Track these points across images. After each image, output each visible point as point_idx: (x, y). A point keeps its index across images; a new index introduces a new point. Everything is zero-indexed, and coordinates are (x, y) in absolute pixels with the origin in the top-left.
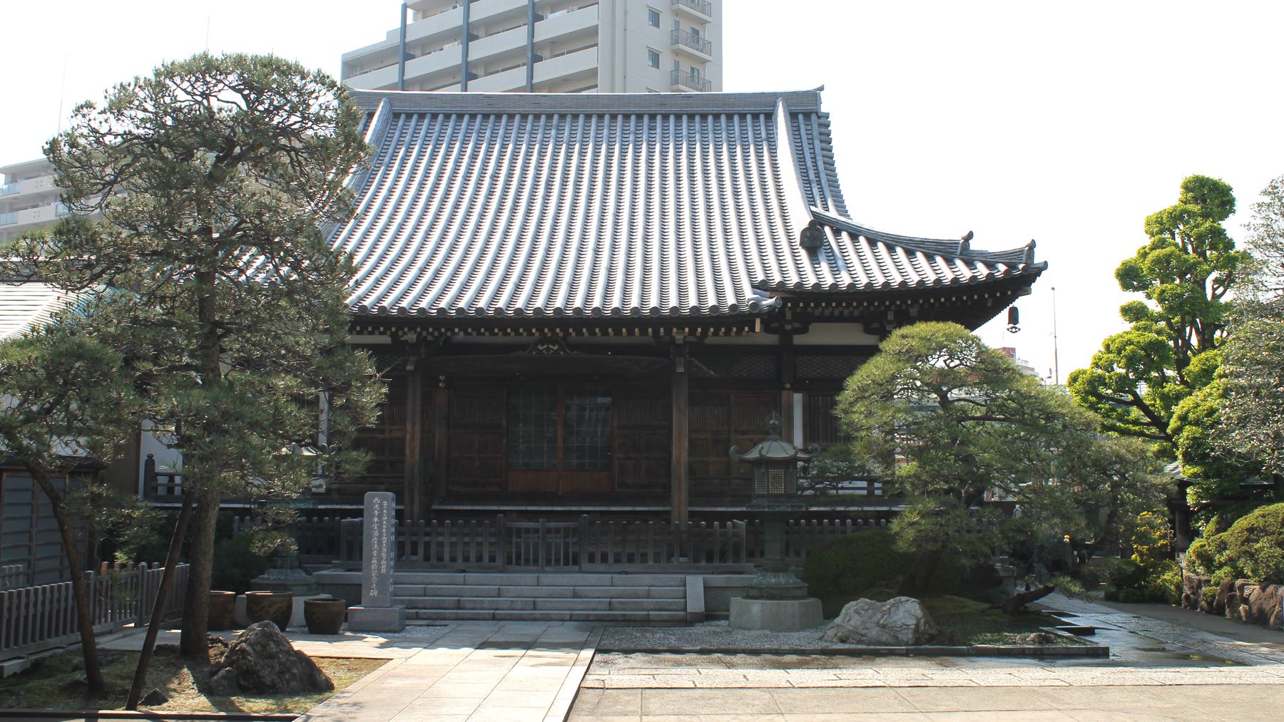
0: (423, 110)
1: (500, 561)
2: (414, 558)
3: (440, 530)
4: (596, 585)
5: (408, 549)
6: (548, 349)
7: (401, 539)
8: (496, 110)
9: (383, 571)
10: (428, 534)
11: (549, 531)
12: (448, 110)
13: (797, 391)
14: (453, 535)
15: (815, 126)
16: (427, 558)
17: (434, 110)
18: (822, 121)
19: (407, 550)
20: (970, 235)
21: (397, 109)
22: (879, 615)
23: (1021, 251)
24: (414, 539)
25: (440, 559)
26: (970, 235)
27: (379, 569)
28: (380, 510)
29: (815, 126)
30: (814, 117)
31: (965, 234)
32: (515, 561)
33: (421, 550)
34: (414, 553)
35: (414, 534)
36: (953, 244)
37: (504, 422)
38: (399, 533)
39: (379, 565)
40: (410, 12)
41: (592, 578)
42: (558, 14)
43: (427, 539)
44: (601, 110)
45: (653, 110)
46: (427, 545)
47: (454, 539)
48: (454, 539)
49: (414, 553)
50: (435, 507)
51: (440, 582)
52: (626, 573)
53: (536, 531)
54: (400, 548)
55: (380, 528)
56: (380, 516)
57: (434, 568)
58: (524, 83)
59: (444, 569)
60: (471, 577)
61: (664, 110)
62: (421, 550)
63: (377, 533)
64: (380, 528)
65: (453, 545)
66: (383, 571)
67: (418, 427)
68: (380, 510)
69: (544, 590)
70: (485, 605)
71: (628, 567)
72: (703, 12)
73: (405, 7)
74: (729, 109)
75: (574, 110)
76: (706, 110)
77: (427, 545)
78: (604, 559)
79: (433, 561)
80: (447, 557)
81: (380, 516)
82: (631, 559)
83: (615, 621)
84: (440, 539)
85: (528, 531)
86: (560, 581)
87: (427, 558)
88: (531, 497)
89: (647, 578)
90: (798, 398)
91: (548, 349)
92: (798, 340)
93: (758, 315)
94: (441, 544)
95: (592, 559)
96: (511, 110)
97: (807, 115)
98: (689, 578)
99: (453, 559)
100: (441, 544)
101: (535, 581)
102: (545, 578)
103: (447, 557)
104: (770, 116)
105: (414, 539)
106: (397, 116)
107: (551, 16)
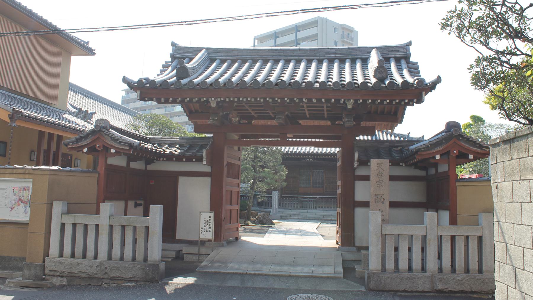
1: (299, 207)
4: (320, 212)
11: (310, 201)
16: (283, 206)
19: (281, 205)
20: (409, 133)
26: (409, 133)
28: (276, 195)
32: (302, 207)
36: (405, 135)
38: (279, 201)
40: (256, 41)
41: (319, 211)
42: (304, 43)
51: (287, 212)
53: (307, 201)
54: (280, 204)
57: (284, 209)
58: (273, 45)
59: (287, 209)
60: (293, 210)
65: (288, 204)
68: (276, 195)
71: (327, 209)
72: (352, 41)
73: (255, 39)
78: (322, 207)
79: (285, 208)
82: (328, 207)
83: (325, 220)
85: (305, 201)
86: (314, 212)
88: (305, 194)
89: (332, 212)
94: (286, 204)
95: (319, 207)
102: (309, 211)
104: (365, 61)
107: (302, 43)
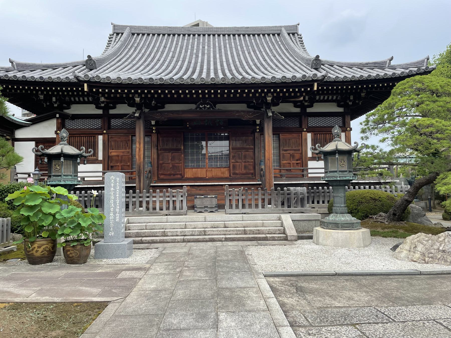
0: (144, 32)
2: (141, 209)
3: (154, 195)
5: (131, 206)
6: (205, 107)
7: (128, 200)
8: (173, 32)
9: (117, 220)
10: (148, 197)
12: (154, 32)
13: (308, 132)
14: (160, 197)
15: (297, 38)
17: (148, 32)
18: (299, 36)
20: (392, 59)
21: (133, 32)
22: (438, 244)
23: (423, 61)
24: (141, 199)
25: (154, 209)
26: (392, 59)
27: (115, 219)
29: (297, 38)
30: (296, 35)
31: (390, 57)
33: (144, 205)
34: (141, 206)
35: (140, 197)
37: (182, 148)
39: (115, 217)
41: (233, 217)
43: (148, 199)
44: (214, 33)
45: (234, 33)
46: (148, 203)
47: (161, 199)
48: (161, 199)
49: (141, 206)
50: (152, 185)
52: (248, 214)
55: (115, 194)
56: (115, 187)
57: (151, 214)
59: (157, 214)
61: (238, 33)
62: (144, 205)
63: (113, 197)
64: (115, 194)
65: (161, 202)
66: (117, 220)
67: (142, 145)
69: (209, 224)
70: (179, 234)
74: (263, 32)
75: (204, 33)
76: (254, 32)
77: (148, 203)
80: (158, 208)
81: (115, 187)
84: (154, 199)
87: (148, 209)
89: (260, 216)
90: (309, 135)
91: (205, 107)
92: (309, 110)
93: (316, 81)
94: (155, 202)
96: (179, 33)
97: (293, 34)
98: (283, 216)
99: (161, 209)
100: (155, 202)
101: (203, 219)
103: (158, 208)
105: (141, 199)
106: (133, 34)
